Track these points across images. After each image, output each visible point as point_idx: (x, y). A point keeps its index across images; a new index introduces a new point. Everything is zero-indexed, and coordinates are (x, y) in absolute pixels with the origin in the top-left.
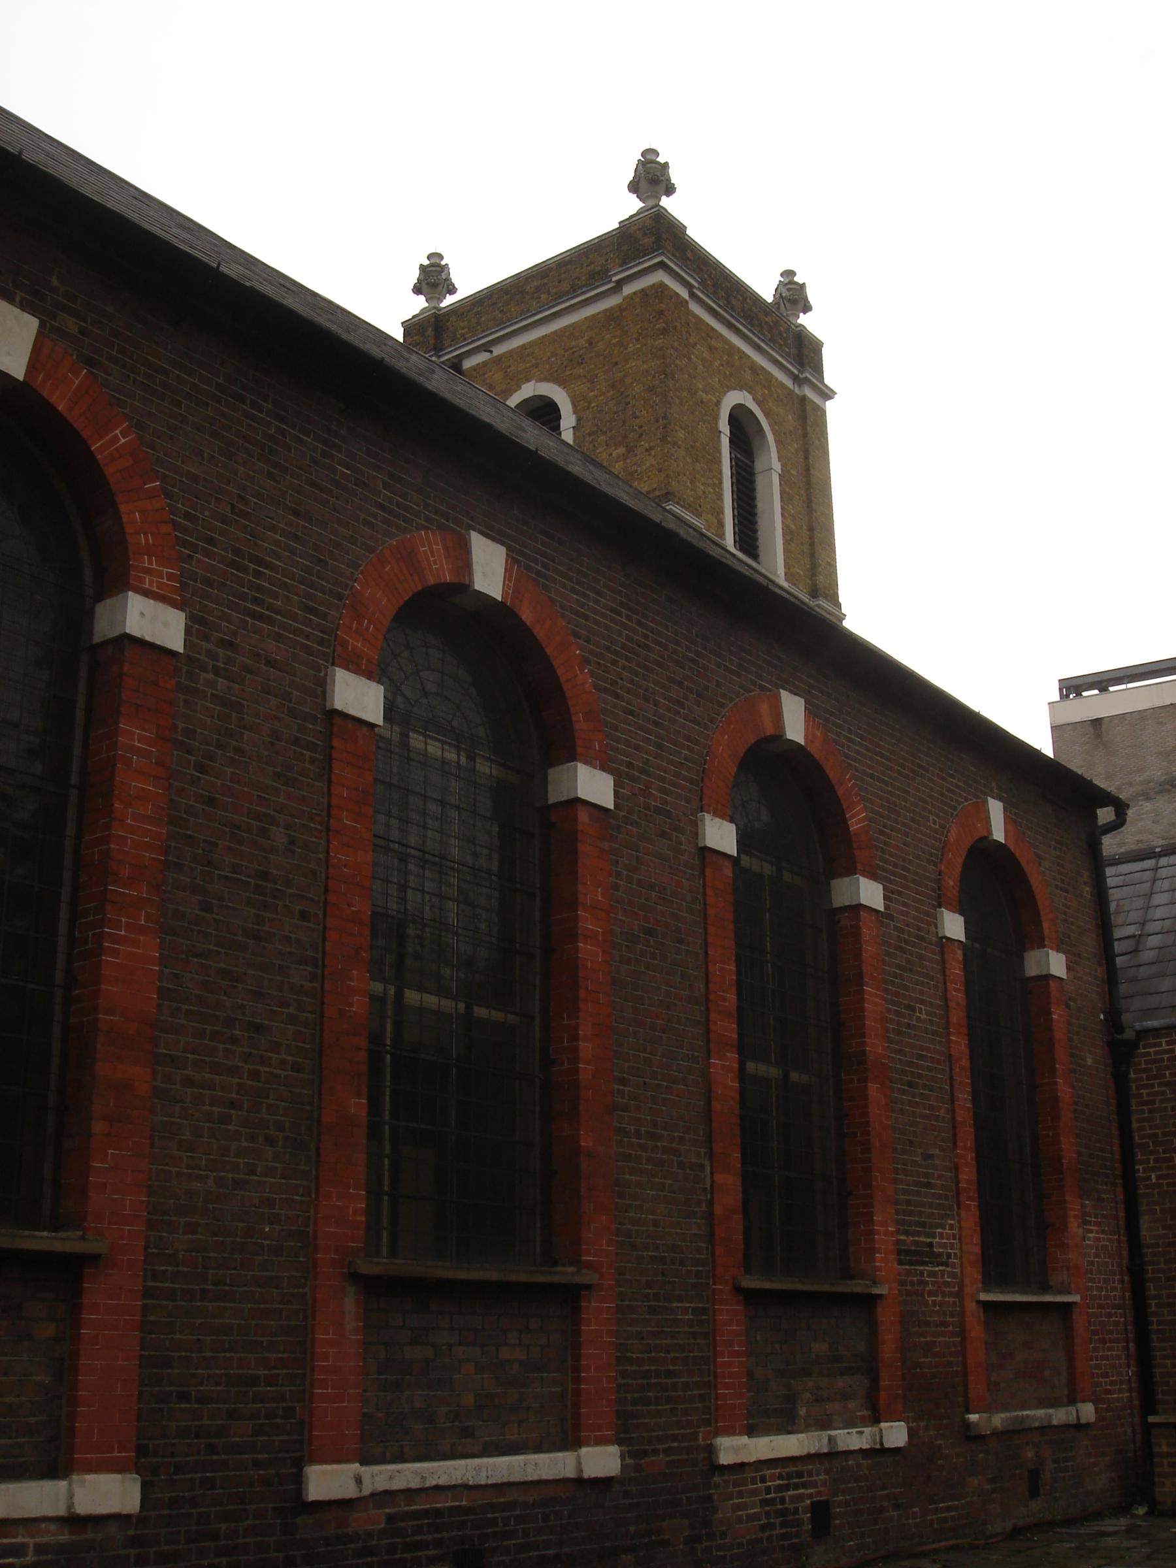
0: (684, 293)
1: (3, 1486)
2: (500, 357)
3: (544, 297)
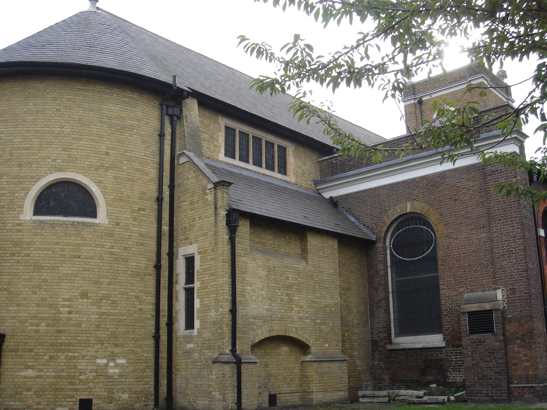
1: (94, 408)
3: (446, 82)
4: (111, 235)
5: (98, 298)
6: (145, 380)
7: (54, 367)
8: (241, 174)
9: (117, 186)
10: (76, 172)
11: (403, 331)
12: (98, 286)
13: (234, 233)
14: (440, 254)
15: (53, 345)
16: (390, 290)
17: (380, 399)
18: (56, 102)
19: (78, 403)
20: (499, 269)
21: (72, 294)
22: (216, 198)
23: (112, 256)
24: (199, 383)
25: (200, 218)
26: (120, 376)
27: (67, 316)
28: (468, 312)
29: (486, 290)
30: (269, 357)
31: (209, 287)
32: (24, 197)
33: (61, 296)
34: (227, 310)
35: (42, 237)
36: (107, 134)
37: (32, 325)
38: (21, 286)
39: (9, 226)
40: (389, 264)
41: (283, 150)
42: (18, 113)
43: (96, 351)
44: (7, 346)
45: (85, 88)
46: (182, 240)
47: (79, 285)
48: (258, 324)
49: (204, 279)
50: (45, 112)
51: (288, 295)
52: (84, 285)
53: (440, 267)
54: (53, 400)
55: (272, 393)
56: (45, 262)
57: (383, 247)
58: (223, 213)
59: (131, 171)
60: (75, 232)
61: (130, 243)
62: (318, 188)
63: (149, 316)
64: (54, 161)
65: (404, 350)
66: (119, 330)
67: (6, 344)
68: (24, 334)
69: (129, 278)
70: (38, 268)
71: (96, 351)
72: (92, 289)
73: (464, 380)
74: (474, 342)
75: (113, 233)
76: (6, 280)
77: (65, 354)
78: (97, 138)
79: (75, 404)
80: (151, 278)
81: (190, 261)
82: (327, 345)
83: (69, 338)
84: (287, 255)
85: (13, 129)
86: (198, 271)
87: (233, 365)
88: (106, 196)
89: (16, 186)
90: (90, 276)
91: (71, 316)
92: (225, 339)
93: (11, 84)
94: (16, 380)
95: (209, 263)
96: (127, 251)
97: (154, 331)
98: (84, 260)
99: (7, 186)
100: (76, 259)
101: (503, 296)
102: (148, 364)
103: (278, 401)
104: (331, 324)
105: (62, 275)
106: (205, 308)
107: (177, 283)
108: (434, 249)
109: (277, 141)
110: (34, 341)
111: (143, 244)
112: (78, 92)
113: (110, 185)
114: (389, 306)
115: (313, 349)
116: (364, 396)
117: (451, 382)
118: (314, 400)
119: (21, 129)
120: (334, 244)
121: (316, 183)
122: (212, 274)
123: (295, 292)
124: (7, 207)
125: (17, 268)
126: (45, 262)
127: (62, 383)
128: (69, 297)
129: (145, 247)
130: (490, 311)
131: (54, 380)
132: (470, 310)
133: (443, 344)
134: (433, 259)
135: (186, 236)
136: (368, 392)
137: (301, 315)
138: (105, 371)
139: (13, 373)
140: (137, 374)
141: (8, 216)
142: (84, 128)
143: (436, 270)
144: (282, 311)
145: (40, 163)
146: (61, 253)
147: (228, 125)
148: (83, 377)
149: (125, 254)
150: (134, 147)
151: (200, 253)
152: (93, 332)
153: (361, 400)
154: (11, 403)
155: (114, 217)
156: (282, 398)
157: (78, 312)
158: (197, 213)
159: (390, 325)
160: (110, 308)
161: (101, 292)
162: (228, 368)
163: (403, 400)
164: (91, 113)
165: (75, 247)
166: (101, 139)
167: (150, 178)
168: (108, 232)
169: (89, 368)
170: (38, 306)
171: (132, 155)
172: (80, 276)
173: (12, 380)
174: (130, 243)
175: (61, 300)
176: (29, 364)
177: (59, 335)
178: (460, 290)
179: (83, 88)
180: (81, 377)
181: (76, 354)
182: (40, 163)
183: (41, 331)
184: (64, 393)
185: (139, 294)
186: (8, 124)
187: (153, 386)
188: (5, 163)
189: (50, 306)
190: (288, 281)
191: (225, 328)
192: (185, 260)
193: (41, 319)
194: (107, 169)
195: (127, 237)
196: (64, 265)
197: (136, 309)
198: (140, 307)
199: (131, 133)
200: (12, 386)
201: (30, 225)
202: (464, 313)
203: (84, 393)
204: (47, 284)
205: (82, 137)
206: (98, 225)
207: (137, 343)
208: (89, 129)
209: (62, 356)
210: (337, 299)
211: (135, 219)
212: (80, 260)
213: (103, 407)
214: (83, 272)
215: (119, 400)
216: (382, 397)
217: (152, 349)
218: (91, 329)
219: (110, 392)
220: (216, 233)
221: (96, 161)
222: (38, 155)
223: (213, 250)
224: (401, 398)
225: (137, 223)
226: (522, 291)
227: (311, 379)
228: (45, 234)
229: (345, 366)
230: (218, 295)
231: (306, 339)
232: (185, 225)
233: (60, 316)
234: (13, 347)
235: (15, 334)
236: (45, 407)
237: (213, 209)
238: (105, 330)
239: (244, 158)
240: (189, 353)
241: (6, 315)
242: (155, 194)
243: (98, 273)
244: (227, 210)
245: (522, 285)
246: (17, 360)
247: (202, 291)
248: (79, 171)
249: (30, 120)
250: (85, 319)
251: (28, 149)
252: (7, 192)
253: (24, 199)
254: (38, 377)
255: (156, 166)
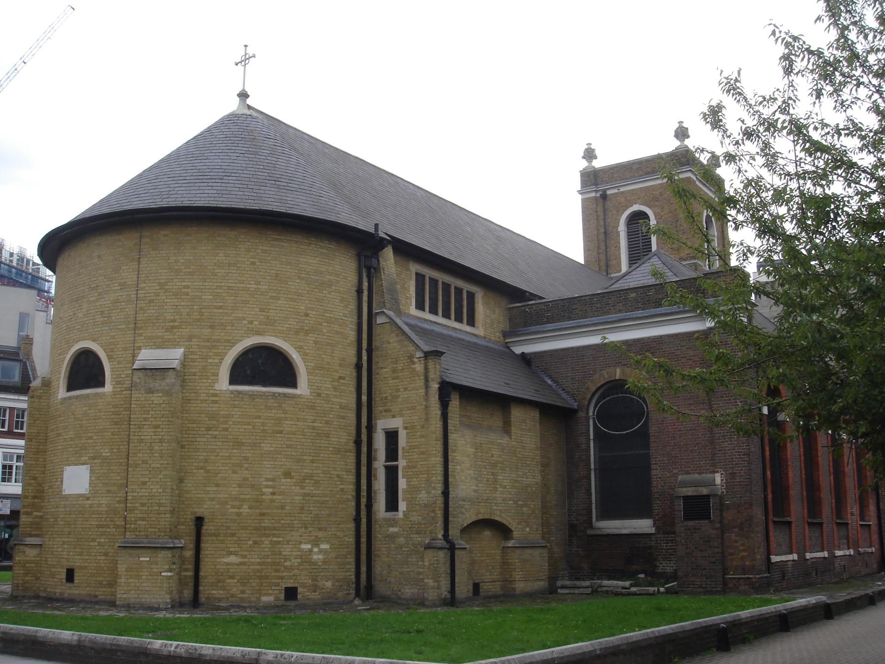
0: (695, 179)
2: (622, 193)
3: (640, 172)
4: (313, 407)
5: (302, 478)
6: (347, 566)
7: (259, 553)
8: (433, 331)
9: (317, 352)
10: (275, 336)
11: (607, 513)
12: (301, 464)
13: (447, 409)
14: (653, 430)
15: (256, 529)
16: (592, 467)
17: (581, 590)
18: (251, 254)
19: (283, 591)
20: (719, 451)
21: (274, 473)
22: (426, 369)
23: (315, 431)
24: (406, 570)
25: (406, 389)
26: (324, 562)
27: (271, 497)
28: (683, 497)
29: (703, 473)
30: (473, 542)
31: (419, 466)
32: (219, 364)
33: (264, 476)
34: (440, 492)
35: (241, 410)
36: (306, 292)
37: (233, 507)
38: (219, 465)
39: (203, 396)
40: (592, 437)
41: (471, 296)
42: (207, 264)
43: (300, 536)
44: (206, 530)
45: (282, 237)
46: (381, 412)
47: (282, 463)
48: (467, 507)
49: (411, 457)
50: (238, 265)
51: (493, 474)
52: (287, 463)
53: (652, 445)
54: (258, 588)
55: (476, 581)
56: (246, 437)
57: (586, 417)
58: (435, 386)
59: (331, 335)
60: (276, 405)
61: (331, 416)
62: (507, 341)
63: (350, 497)
64: (251, 322)
65: (608, 535)
66: (322, 512)
67: (205, 528)
68: (225, 517)
69: (331, 456)
70: (239, 444)
71: (300, 536)
72: (295, 467)
73: (676, 570)
74: (688, 530)
75: (316, 405)
76: (203, 458)
77: (270, 539)
78: (296, 297)
79: (280, 593)
80: (352, 454)
81: (392, 437)
82: (528, 529)
83: (273, 521)
84: (490, 428)
85: (201, 284)
86: (403, 448)
87: (446, 550)
88: (307, 364)
89: (208, 350)
90: (293, 453)
91: (275, 497)
92: (437, 523)
93: (195, 229)
94: (218, 567)
95: (419, 440)
96: (328, 425)
97: (354, 513)
98: (286, 436)
99: (198, 350)
100: (278, 435)
101: (722, 480)
102: (349, 550)
103: (481, 590)
104: (532, 506)
105: (264, 452)
106: (412, 490)
107: (375, 459)
108: (646, 422)
109: (466, 287)
110: (236, 525)
111: (343, 417)
112: (274, 243)
113: (311, 351)
114: (590, 485)
115: (515, 534)
116: (563, 587)
117: (661, 572)
118: (517, 589)
119: (210, 284)
120: (535, 414)
121: (505, 334)
122: (423, 453)
123: (500, 471)
124: (200, 374)
125: (214, 444)
126: (246, 437)
127: (267, 570)
128: (272, 477)
129: (345, 421)
130: (707, 497)
131: (258, 567)
132: (686, 494)
133: (653, 531)
134: (643, 435)
135: (387, 408)
136: (568, 583)
137: (505, 496)
138: (309, 557)
139: (214, 560)
140: (340, 560)
141: (200, 384)
142: (282, 285)
143: (647, 447)
144: (488, 492)
145: (235, 325)
146: (262, 428)
147: (419, 272)
148: (287, 564)
149: (327, 429)
150: (333, 306)
151: (406, 428)
152: (296, 515)
153: (559, 591)
154: (213, 592)
155: (315, 388)
156: (485, 587)
157: (281, 493)
158: (402, 383)
159: (591, 507)
160: (313, 488)
161: (305, 471)
162: (442, 556)
163: (607, 591)
164: (289, 267)
165: (277, 422)
166: (300, 297)
167: (349, 341)
168: (310, 404)
169: (294, 553)
170: (239, 486)
171: (332, 316)
172: (283, 453)
173: (214, 567)
174: (331, 416)
175: (264, 479)
176: (231, 549)
177: (263, 518)
178: (675, 471)
179: (278, 237)
180: (286, 564)
181: (281, 539)
182: (235, 325)
183: (243, 514)
184: (269, 581)
185: (340, 473)
186: (194, 277)
187: (353, 574)
188: (194, 323)
189: (253, 486)
190: (494, 459)
191: (438, 512)
192: (384, 434)
193: (244, 500)
194: (307, 333)
195: (328, 409)
196: (265, 441)
197: (338, 489)
198: (342, 487)
199: (330, 290)
200: (214, 574)
201: (227, 395)
202: (678, 497)
203: (289, 581)
204: (248, 462)
205: (280, 295)
206: (299, 396)
207: (339, 526)
208: (287, 286)
209: (266, 541)
210: (538, 478)
211: (335, 389)
212: (282, 435)
213: (308, 595)
214: (286, 449)
215: (323, 589)
216: (584, 587)
217: (352, 533)
218: (295, 511)
219: (315, 579)
220: (426, 407)
221: (295, 323)
222: (233, 315)
223: (423, 427)
224: (604, 589)
225: (338, 394)
226: (742, 476)
227: (513, 567)
228: (245, 406)
229: (545, 552)
230: (430, 476)
231: (510, 523)
232: (385, 395)
233: (264, 497)
234: (213, 532)
235: (215, 517)
236: (250, 596)
237: (423, 381)
238: (309, 512)
239: (434, 311)
240: (392, 537)
241: (204, 496)
242: (354, 360)
243: (301, 450)
244: (439, 383)
245: (742, 470)
246: (217, 545)
247: (409, 470)
248: (278, 335)
249: (221, 274)
250: (289, 501)
251: (221, 308)
252: (198, 357)
253: (218, 365)
254: (241, 564)
255: (354, 327)
